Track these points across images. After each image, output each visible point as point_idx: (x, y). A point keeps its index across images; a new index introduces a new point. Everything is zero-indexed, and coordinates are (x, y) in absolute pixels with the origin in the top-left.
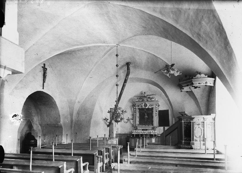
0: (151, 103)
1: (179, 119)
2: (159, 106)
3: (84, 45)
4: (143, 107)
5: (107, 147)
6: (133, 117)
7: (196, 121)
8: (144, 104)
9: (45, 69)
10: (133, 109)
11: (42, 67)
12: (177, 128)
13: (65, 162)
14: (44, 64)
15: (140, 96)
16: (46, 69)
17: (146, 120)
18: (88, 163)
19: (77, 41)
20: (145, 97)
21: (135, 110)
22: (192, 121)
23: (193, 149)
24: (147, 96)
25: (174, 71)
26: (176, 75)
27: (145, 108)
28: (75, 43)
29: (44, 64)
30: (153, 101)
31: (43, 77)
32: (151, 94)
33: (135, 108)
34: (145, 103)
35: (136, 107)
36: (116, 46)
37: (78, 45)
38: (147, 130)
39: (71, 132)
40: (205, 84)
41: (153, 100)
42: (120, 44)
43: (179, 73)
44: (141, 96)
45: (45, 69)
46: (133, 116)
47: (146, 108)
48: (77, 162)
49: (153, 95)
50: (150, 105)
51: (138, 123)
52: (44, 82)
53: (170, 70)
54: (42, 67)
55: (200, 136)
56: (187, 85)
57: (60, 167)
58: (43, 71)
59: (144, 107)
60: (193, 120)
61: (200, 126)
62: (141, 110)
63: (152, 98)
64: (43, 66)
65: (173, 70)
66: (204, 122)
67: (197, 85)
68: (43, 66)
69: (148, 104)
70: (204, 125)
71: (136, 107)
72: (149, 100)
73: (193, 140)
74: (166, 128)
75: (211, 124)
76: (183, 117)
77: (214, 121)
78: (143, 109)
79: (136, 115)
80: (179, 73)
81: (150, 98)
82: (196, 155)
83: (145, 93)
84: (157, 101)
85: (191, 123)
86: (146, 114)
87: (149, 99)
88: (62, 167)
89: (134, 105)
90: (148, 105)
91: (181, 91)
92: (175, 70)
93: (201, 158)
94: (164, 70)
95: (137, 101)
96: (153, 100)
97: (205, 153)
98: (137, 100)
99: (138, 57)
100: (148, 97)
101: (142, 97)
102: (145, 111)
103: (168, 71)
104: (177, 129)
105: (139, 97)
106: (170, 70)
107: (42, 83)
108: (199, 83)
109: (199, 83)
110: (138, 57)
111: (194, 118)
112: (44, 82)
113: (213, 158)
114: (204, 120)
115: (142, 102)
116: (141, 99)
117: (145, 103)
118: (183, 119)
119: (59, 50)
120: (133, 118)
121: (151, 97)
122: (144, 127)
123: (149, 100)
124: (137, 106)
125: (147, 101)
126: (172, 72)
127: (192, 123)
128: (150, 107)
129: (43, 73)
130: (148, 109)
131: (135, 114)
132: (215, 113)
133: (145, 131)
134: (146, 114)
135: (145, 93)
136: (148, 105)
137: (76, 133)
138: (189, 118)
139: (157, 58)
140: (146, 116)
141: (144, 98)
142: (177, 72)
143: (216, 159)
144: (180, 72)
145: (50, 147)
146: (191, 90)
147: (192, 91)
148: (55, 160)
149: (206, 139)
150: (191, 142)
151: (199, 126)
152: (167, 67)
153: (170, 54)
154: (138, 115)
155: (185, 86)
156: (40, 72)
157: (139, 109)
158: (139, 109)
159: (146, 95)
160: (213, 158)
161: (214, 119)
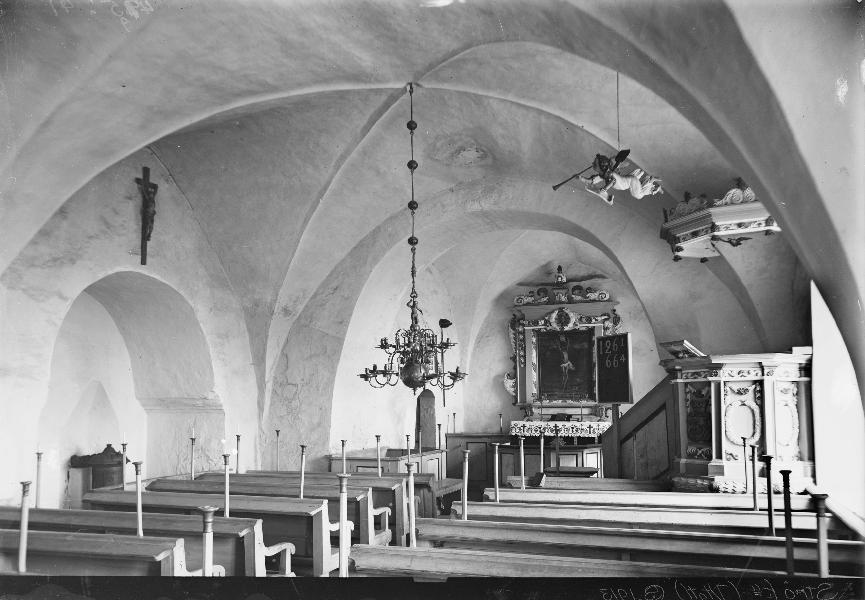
0: (587, 309)
1: (668, 371)
2: (617, 320)
3: (274, 89)
4: (555, 325)
5: (385, 484)
6: (515, 368)
7: (731, 379)
8: (554, 315)
9: (147, 193)
10: (512, 336)
11: (138, 181)
12: (663, 407)
13: (181, 542)
14: (146, 171)
15: (542, 284)
16: (155, 187)
17: (565, 379)
18: (290, 548)
19: (245, 76)
20: (560, 285)
21: (521, 337)
22: (714, 378)
23: (716, 490)
24: (569, 281)
25: (630, 180)
26: (640, 192)
27: (563, 333)
28: (243, 86)
29: (146, 171)
30: (594, 301)
31: (140, 217)
32: (583, 273)
33: (523, 333)
34: (561, 310)
35: (524, 325)
36: (408, 88)
37: (252, 93)
38: (568, 418)
39: (260, 428)
40: (763, 228)
41: (593, 296)
42: (420, 82)
43: (650, 185)
44: (547, 284)
45: (147, 193)
46: (516, 362)
47: (566, 328)
48: (240, 541)
49: (591, 277)
50: (580, 319)
51: (535, 391)
52: (146, 237)
53: (615, 176)
54: (138, 181)
55: (744, 439)
56: (695, 235)
57: (159, 558)
58: (140, 196)
59: (555, 326)
60: (721, 372)
61: (749, 398)
62: (546, 340)
63: (590, 290)
64: (140, 176)
65: (627, 175)
66: (761, 383)
67: (730, 232)
68: (140, 176)
69: (571, 315)
70: (762, 392)
71: (524, 325)
72: (579, 298)
73: (719, 456)
74: (624, 408)
75: (793, 386)
76: (679, 364)
77: (806, 379)
78: (553, 335)
79: (524, 357)
80: (650, 185)
81: (579, 288)
82: (563, 495)
83: (560, 268)
84: (608, 301)
85: (710, 386)
86: (566, 356)
87: (576, 292)
88: (167, 559)
89: (515, 322)
90: (573, 320)
91: (677, 259)
92: (633, 176)
93: (676, 525)
94: (592, 177)
95: (528, 304)
96: (593, 296)
97: (752, 506)
98: (530, 299)
99: (501, 131)
100: (575, 284)
101: (548, 287)
102: (562, 344)
103: (608, 180)
104: (662, 415)
105: (537, 285)
106: (615, 176)
107: (138, 242)
108: (740, 225)
109: (740, 225)
110: (501, 131)
111: (719, 366)
112: (146, 237)
113: (767, 526)
114: (763, 375)
115: (553, 307)
116: (546, 293)
117: (561, 310)
118: (680, 370)
119: (167, 115)
120: (513, 371)
121: (585, 284)
122: (556, 405)
123: (579, 298)
124: (529, 325)
125: (570, 301)
126: (621, 184)
127: (713, 385)
128: (582, 327)
129: (139, 200)
130: (575, 333)
131: (522, 353)
132: (808, 342)
133: (560, 424)
134: (566, 356)
135: (560, 268)
136: (573, 318)
137: (278, 432)
138: (703, 366)
139: (574, 132)
140: (567, 365)
141: (555, 292)
142: (643, 181)
143: (777, 530)
144: (657, 185)
145: (216, 488)
146: (717, 254)
147: (721, 257)
148: (146, 532)
149: (439, 425)
150: (715, 462)
151: (743, 398)
152: (600, 162)
153: (414, 109)
154: (533, 357)
155: (685, 239)
156: (130, 198)
157: (538, 333)
158: (538, 333)
159: (565, 280)
160: (767, 526)
161: (807, 369)
